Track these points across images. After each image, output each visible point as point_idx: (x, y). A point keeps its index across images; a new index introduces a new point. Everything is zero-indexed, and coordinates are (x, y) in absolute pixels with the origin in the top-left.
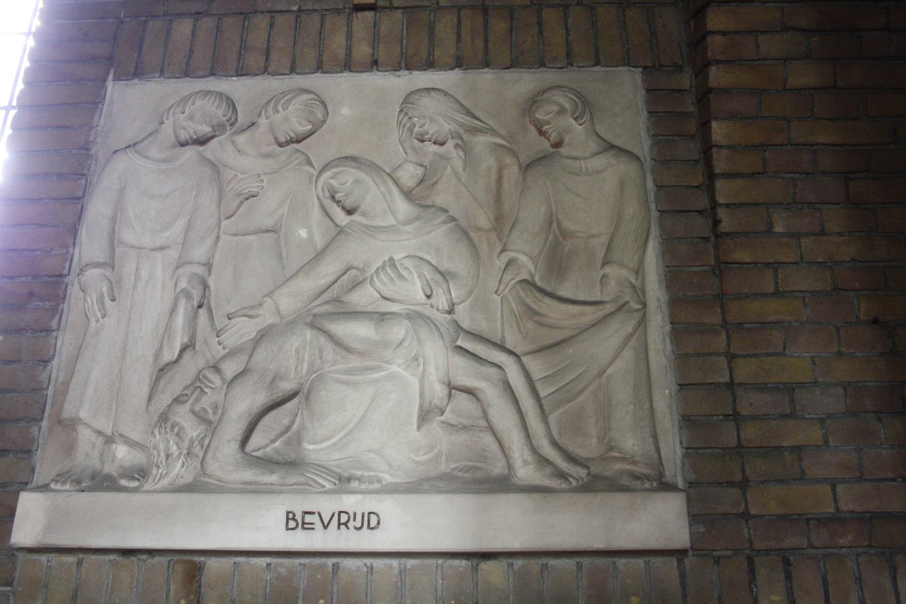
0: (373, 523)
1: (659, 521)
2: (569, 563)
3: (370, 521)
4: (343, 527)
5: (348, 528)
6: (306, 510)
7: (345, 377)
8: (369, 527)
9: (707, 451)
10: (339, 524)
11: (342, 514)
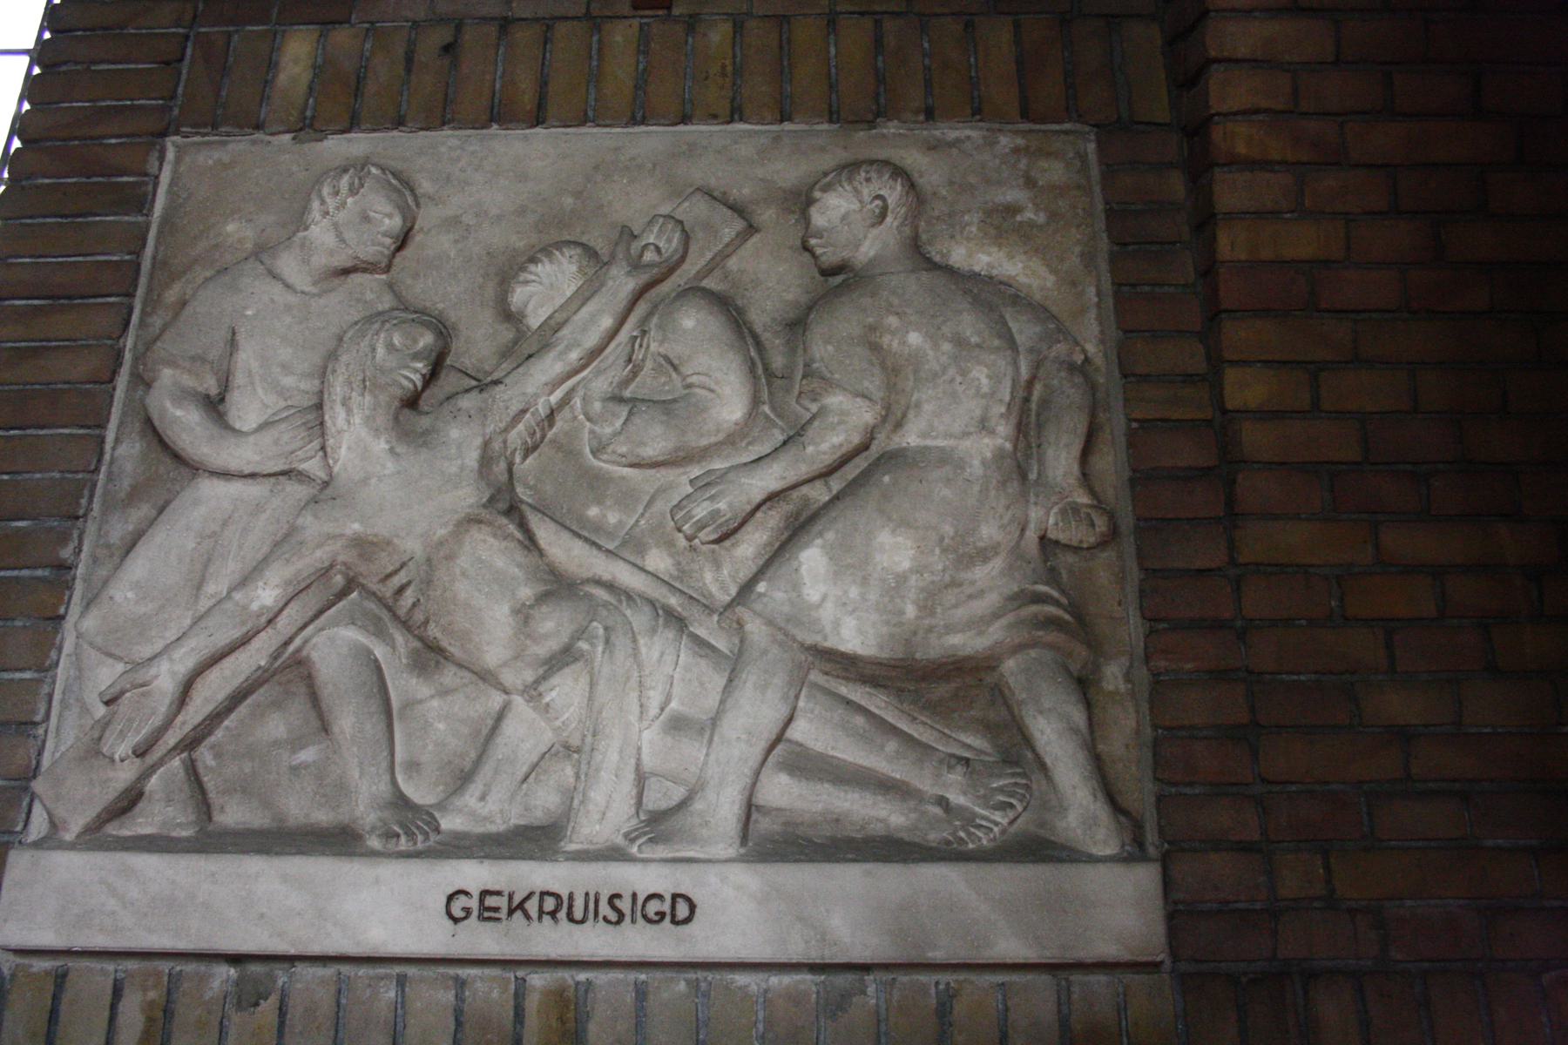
0: (682, 910)
1: (1118, 908)
2: (1099, 979)
3: (455, 908)
4: (546, 918)
5: (528, 917)
6: (490, 887)
7: (760, 371)
8: (571, 919)
9: (1374, 315)
10: (541, 912)
11: (680, 900)
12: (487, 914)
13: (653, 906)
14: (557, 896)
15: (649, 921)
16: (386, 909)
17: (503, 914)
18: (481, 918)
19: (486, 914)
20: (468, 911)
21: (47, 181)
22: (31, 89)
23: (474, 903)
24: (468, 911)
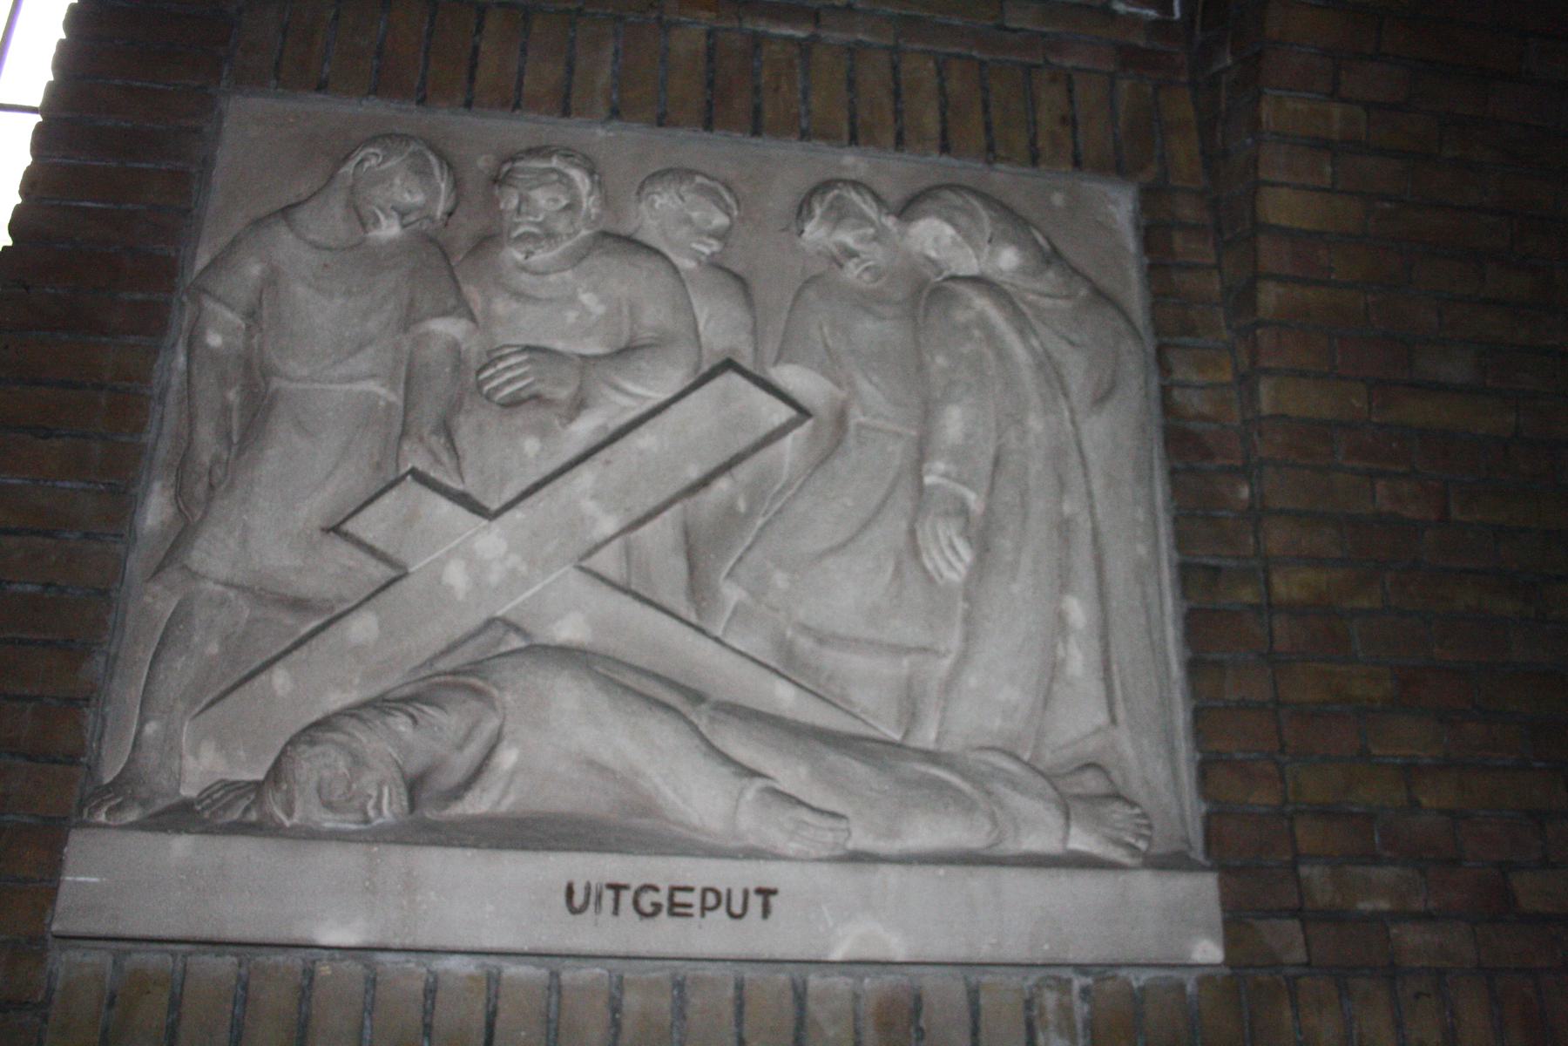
6: (682, 883)
12: (676, 909)
13: (646, 901)
14: (717, 893)
15: (643, 915)
16: (484, 908)
17: (696, 910)
18: (672, 914)
19: (678, 910)
20: (657, 907)
21: (144, 165)
22: (42, 141)
23: (662, 898)
24: (657, 907)
